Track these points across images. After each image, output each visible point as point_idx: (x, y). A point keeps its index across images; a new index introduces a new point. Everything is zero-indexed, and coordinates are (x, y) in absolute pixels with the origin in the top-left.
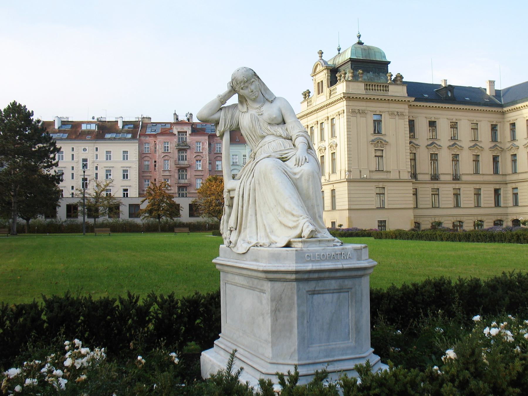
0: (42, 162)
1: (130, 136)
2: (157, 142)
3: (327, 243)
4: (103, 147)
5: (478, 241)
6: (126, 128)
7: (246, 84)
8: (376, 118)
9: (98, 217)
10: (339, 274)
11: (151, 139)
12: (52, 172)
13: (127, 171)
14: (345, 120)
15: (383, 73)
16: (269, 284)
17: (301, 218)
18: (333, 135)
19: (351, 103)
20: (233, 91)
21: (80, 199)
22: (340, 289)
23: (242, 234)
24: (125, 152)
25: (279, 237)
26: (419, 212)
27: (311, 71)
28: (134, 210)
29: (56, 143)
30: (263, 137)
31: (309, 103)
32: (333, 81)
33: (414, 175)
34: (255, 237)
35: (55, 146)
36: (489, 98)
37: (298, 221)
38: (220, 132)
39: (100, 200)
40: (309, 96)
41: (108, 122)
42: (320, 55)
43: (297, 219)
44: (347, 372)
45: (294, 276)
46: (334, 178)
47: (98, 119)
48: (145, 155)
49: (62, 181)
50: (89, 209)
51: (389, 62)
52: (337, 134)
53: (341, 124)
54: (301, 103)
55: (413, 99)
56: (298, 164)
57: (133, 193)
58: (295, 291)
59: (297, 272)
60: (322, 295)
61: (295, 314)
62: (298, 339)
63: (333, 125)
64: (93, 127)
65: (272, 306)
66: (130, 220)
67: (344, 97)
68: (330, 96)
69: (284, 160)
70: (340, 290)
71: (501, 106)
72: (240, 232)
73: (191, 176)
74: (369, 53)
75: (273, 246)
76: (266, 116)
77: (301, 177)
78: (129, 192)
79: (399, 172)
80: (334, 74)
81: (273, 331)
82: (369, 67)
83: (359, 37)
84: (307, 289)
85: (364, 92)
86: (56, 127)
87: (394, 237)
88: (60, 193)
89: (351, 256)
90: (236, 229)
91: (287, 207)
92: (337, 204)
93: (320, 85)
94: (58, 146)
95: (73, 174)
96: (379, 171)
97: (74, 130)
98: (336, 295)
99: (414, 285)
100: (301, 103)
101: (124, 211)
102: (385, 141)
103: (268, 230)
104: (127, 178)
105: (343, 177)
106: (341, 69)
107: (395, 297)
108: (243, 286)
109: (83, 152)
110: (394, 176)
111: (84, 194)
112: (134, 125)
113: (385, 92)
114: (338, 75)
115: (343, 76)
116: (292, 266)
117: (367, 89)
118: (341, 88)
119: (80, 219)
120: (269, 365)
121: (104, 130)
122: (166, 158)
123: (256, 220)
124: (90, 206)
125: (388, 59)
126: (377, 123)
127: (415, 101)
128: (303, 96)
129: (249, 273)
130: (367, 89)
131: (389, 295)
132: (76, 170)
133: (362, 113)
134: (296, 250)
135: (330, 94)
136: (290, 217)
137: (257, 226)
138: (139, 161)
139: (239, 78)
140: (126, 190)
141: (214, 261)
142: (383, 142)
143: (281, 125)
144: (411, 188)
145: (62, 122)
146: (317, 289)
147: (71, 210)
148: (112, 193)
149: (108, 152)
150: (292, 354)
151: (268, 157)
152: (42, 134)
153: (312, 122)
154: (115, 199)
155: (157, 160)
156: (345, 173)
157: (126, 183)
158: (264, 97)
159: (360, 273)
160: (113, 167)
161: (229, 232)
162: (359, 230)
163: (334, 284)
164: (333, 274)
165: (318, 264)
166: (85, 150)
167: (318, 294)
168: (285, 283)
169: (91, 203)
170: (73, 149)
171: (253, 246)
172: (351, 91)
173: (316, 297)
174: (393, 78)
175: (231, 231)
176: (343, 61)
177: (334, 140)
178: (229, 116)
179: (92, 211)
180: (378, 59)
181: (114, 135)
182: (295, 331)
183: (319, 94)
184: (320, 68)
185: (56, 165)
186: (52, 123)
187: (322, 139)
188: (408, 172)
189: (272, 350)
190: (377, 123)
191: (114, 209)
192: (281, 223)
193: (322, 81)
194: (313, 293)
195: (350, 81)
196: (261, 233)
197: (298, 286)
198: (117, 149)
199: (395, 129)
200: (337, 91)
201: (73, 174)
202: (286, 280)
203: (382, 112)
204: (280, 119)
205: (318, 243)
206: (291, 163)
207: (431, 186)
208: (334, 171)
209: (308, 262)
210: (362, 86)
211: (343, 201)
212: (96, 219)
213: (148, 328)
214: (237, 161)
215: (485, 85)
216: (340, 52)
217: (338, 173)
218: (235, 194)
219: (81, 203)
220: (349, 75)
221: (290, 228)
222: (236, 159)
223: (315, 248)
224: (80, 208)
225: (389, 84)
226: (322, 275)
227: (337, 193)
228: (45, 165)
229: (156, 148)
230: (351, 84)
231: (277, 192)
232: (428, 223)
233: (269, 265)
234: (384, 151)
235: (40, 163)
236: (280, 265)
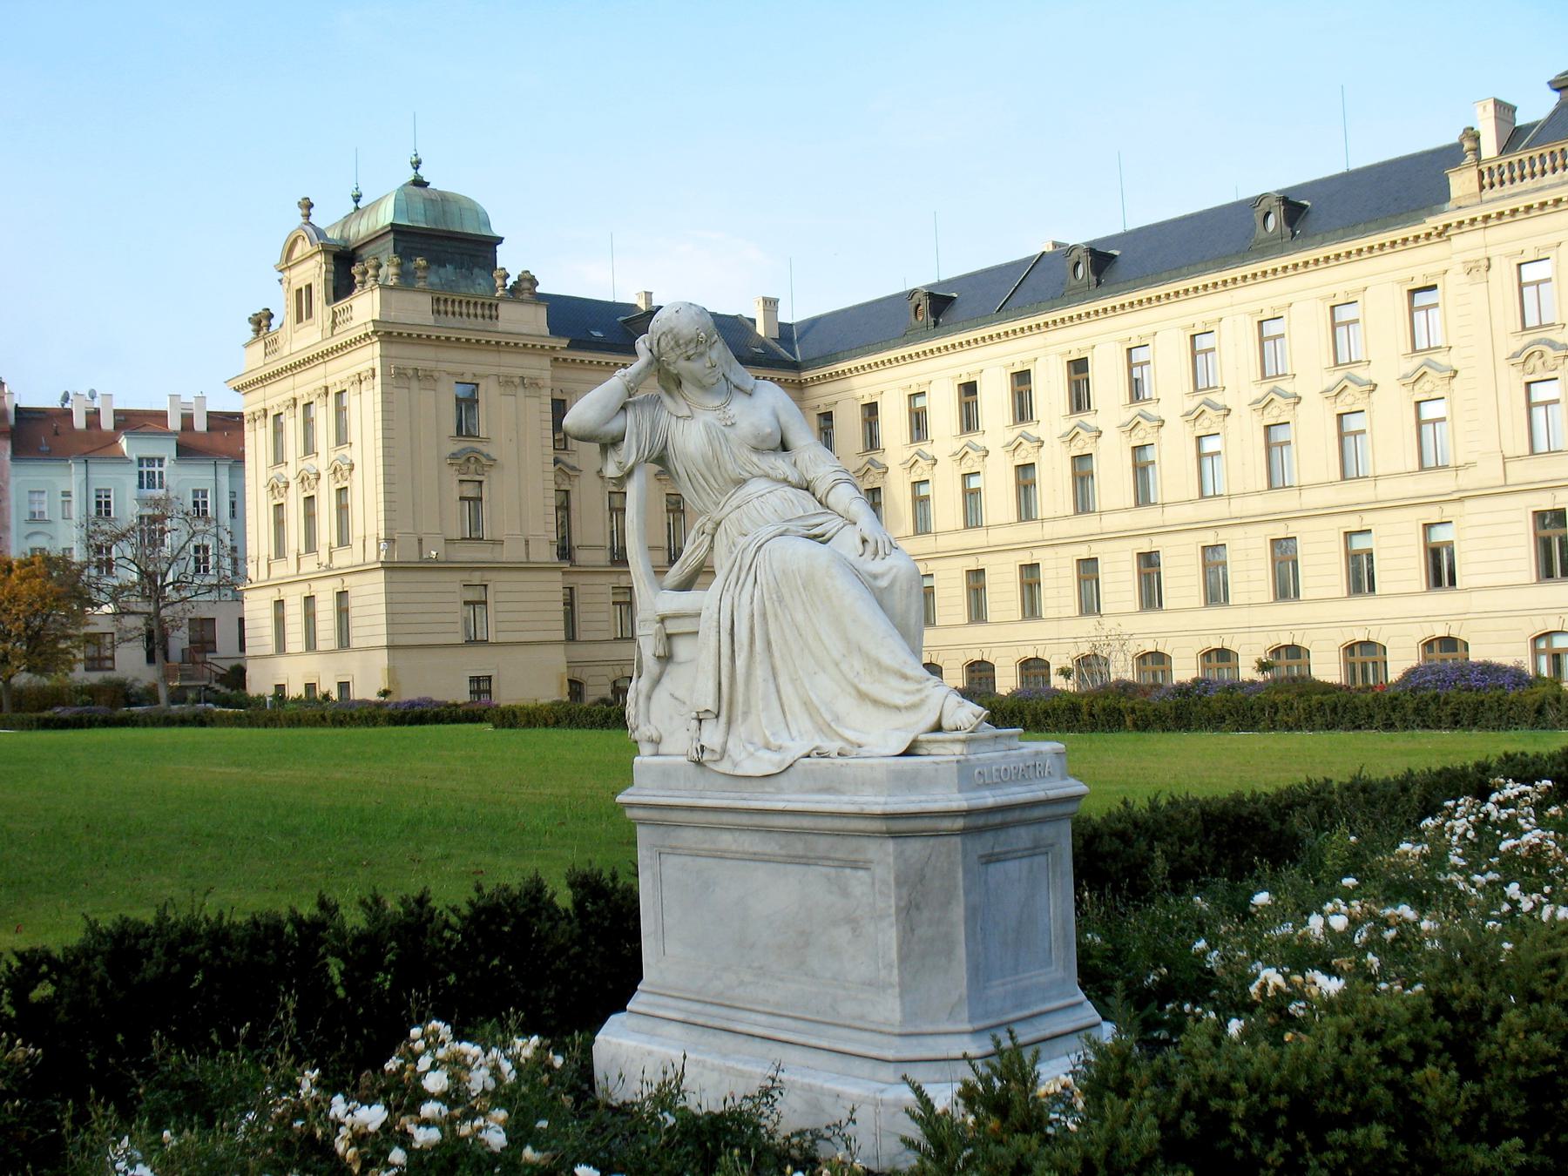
5: (145, 725)
7: (701, 348)
10: (1037, 813)
14: (379, 398)
16: (890, 845)
18: (341, 438)
19: (395, 350)
26: (580, 652)
27: (276, 256)
30: (741, 482)
31: (271, 348)
33: (565, 551)
36: (763, 344)
37: (919, 691)
40: (269, 326)
44: (1040, 1046)
45: (959, 823)
46: (343, 559)
51: (500, 240)
52: (354, 434)
53: (366, 409)
54: (247, 346)
55: (565, 342)
58: (959, 857)
59: (968, 813)
61: (958, 912)
63: (340, 411)
67: (375, 332)
68: (333, 328)
71: (796, 367)
72: (729, 723)
74: (444, 212)
79: (527, 542)
80: (344, 268)
81: (903, 958)
82: (442, 249)
83: (417, 165)
84: (981, 852)
90: (717, 716)
91: (886, 659)
92: (353, 632)
93: (303, 298)
100: (247, 346)
102: (488, 457)
105: (371, 555)
106: (364, 252)
108: (756, 858)
110: (512, 552)
114: (356, 269)
115: (371, 272)
117: (439, 312)
118: (365, 306)
120: (897, 1041)
126: (467, 404)
127: (570, 347)
128: (251, 327)
129: (838, 824)
130: (439, 312)
133: (425, 377)
136: (894, 682)
137: (782, 706)
139: (685, 331)
141: (620, 798)
142: (484, 460)
146: (997, 850)
153: (279, 400)
161: (695, 723)
162: (438, 704)
167: (998, 861)
168: (932, 841)
172: (393, 316)
173: (992, 868)
174: (510, 282)
175: (700, 721)
176: (371, 230)
177: (346, 451)
178: (647, 426)
180: (470, 228)
182: (961, 952)
183: (299, 320)
184: (303, 248)
187: (309, 449)
188: (551, 542)
189: (903, 1004)
190: (467, 404)
193: (309, 287)
194: (990, 859)
195: (391, 288)
196: (801, 722)
197: (964, 844)
200: (354, 314)
202: (936, 834)
203: (482, 377)
207: (613, 580)
208: (343, 540)
210: (425, 302)
211: (371, 622)
214: (45, 508)
215: (758, 314)
216: (360, 205)
217: (357, 545)
220: (389, 272)
221: (898, 708)
222: (41, 503)
225: (501, 299)
227: (353, 603)
230: (395, 295)
232: (605, 680)
233: (895, 799)
236: (923, 798)
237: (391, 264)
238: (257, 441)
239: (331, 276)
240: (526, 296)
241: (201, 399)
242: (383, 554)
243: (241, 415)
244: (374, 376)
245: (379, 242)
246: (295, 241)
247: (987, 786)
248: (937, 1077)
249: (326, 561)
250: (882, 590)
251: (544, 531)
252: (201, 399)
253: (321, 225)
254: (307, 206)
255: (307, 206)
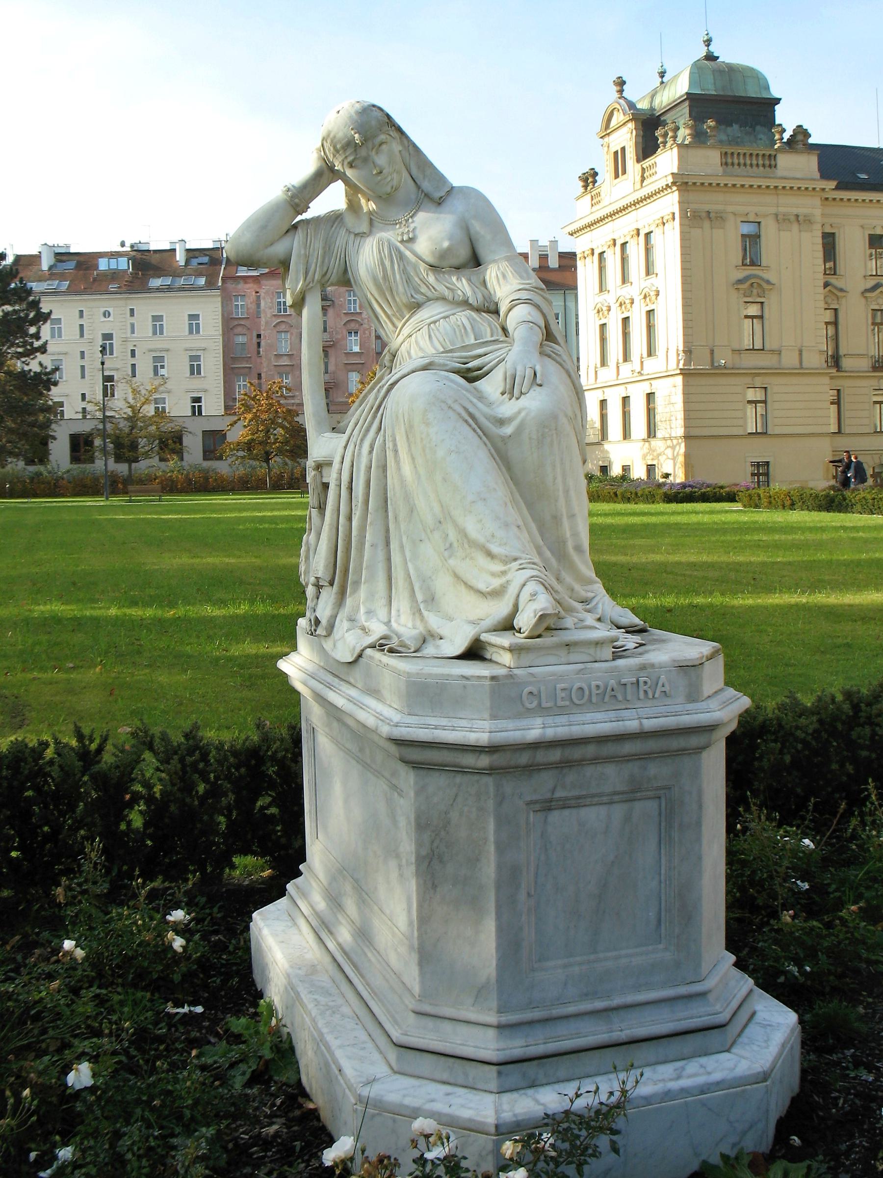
0: (12, 345)
1: (202, 281)
2: (262, 293)
3: (591, 651)
4: (146, 307)
6: (195, 262)
8: (746, 229)
9: (136, 460)
11: (248, 286)
12: (34, 366)
13: (198, 358)
15: (763, 125)
17: (515, 565)
20: (327, 173)
21: (96, 422)
22: (633, 791)
23: (349, 601)
24: (194, 317)
25: (451, 619)
27: (597, 124)
28: (214, 442)
29: (39, 302)
31: (595, 200)
32: (648, 147)
33: (836, 361)
34: (382, 613)
35: (38, 310)
37: (504, 573)
38: (292, 293)
39: (140, 424)
40: (595, 182)
41: (155, 251)
42: (619, 88)
43: (503, 568)
45: (484, 761)
47: (132, 246)
48: (236, 323)
49: (56, 384)
50: (118, 444)
51: (778, 101)
52: (658, 267)
55: (833, 184)
56: (511, 391)
57: (214, 405)
58: (490, 804)
59: (492, 749)
60: (574, 811)
62: (498, 948)
64: (123, 264)
65: (419, 844)
66: (207, 464)
67: (674, 183)
68: (642, 181)
69: (471, 375)
70: (632, 793)
73: (336, 365)
75: (430, 650)
76: (424, 246)
77: (520, 430)
78: (203, 404)
79: (801, 352)
80: (650, 130)
85: (720, 170)
86: (45, 266)
87: (788, 503)
88: (55, 409)
89: (667, 688)
90: (331, 584)
91: (472, 528)
93: (619, 158)
94: (45, 308)
95: (83, 367)
96: (753, 349)
97: (80, 270)
98: (618, 811)
99: (848, 695)
100: (578, 198)
101: (193, 445)
103: (420, 597)
104: (199, 373)
107: (799, 733)
109: (103, 319)
110: (789, 360)
111: (104, 409)
112: (210, 257)
113: (768, 169)
114: (658, 133)
115: (670, 134)
116: (477, 729)
117: (726, 164)
118: (667, 161)
119: (99, 465)
121: (146, 268)
122: (283, 327)
123: (389, 559)
124: (118, 437)
125: (775, 93)
126: (751, 244)
127: (837, 188)
128: (581, 184)
130: (726, 164)
131: (780, 725)
132: (81, 359)
133: (714, 218)
134: (493, 678)
135: (643, 179)
136: (482, 560)
138: (224, 334)
140: (197, 400)
143: (467, 272)
144: (827, 388)
145: (57, 254)
146: (559, 794)
147: (80, 445)
148: (167, 406)
149: (157, 318)
150: (479, 991)
151: (425, 368)
152: (10, 285)
154: (172, 421)
155: (262, 333)
156: (678, 355)
157: (196, 384)
158: (418, 187)
159: (694, 741)
160: (168, 350)
163: (613, 777)
164: (611, 749)
165: (563, 719)
166: (106, 314)
167: (564, 807)
168: (459, 779)
169: (121, 430)
170: (81, 312)
171: (372, 646)
173: (555, 816)
174: (786, 136)
176: (671, 100)
178: (318, 245)
179: (125, 448)
180: (752, 92)
181: (168, 281)
183: (617, 176)
184: (618, 118)
185: (43, 349)
186: (34, 259)
190: (751, 244)
191: (170, 441)
192: (457, 576)
193: (623, 149)
194: (548, 806)
196: (402, 603)
198: (175, 311)
199: (792, 256)
201: (83, 367)
202: (461, 770)
204: (463, 253)
205: (563, 653)
206: (492, 386)
209: (529, 713)
212: (134, 465)
213: (129, 823)
216: (665, 80)
218: (331, 477)
219: (98, 430)
220: (684, 134)
223: (554, 669)
224: (98, 442)
226: (577, 753)
228: (20, 350)
229: (258, 305)
231: (445, 480)
234: (765, 305)
235: (9, 348)
236: (444, 722)
237: (686, 126)
238: (586, 273)
239: (640, 139)
240: (800, 146)
241: (554, 243)
242: (682, 362)
243: (574, 255)
244: (674, 219)
245: (678, 109)
246: (611, 114)
247: (541, 710)
248: (445, 1076)
249: (639, 369)
250: (505, 439)
251: (817, 342)
252: (554, 243)
253: (633, 98)
254: (621, 83)
255: (621, 83)
